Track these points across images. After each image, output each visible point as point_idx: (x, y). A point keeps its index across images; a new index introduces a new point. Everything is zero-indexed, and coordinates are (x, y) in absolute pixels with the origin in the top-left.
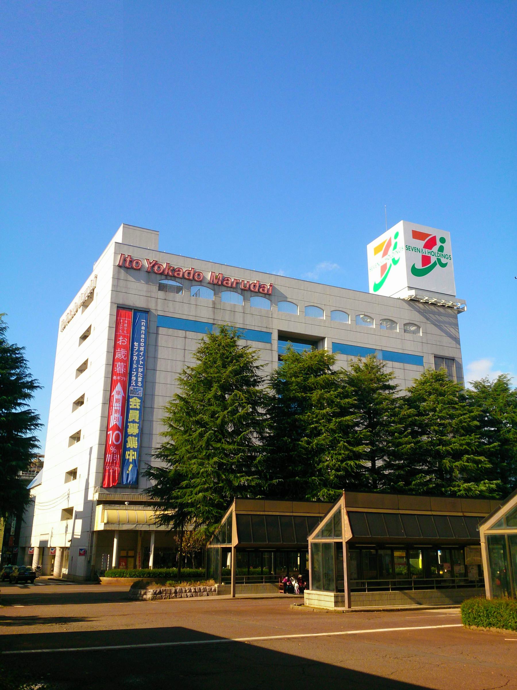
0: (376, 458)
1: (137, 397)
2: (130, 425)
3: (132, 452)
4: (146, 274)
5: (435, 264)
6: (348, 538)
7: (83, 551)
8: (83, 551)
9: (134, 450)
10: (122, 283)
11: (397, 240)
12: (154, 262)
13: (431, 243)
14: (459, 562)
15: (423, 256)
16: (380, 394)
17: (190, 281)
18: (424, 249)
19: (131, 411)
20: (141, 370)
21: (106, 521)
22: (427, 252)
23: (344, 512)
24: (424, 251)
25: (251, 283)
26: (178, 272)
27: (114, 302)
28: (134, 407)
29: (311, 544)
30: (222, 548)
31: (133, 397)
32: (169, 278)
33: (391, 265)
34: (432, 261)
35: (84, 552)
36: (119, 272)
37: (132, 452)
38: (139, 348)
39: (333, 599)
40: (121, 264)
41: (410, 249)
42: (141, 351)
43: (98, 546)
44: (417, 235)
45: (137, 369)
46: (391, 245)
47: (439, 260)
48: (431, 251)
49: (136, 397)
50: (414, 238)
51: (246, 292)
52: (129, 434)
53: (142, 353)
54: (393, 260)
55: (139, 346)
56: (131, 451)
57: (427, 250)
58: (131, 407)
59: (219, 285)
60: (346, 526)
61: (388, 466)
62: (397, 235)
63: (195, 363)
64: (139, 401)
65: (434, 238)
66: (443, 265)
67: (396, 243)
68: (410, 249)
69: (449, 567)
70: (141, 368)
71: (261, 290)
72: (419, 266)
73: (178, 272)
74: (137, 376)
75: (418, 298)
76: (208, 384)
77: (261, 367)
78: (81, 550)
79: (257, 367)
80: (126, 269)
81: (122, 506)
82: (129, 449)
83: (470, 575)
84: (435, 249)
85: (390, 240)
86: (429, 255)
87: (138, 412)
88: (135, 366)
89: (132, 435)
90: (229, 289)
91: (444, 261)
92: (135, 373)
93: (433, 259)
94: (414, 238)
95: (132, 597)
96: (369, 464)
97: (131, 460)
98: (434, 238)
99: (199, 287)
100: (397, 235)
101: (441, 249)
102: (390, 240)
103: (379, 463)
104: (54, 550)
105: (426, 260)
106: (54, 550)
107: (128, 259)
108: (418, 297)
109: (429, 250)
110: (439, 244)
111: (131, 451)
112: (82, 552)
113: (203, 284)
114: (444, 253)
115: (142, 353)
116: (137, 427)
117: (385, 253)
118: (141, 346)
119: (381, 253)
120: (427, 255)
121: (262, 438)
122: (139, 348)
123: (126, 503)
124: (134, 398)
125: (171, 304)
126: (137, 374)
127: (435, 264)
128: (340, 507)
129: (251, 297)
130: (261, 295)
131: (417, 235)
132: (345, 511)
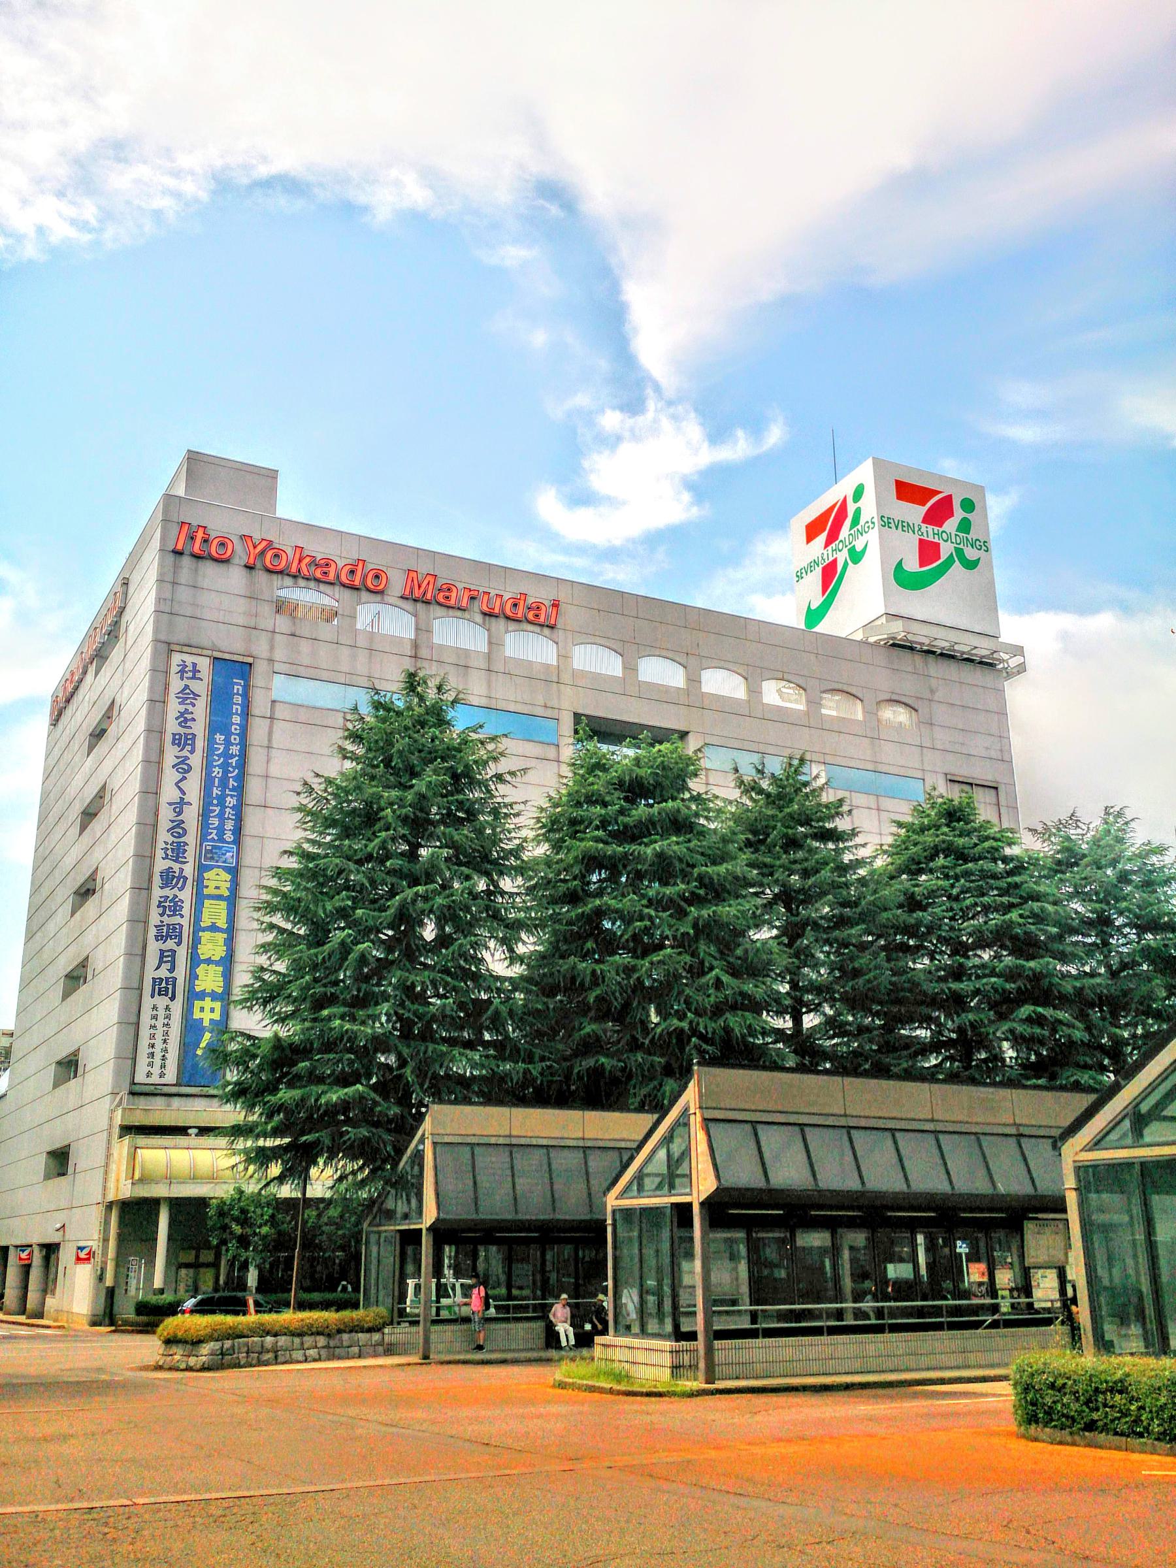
0: (804, 1010)
1: (225, 869)
2: (205, 936)
3: (208, 1003)
4: (244, 571)
5: (950, 561)
6: (706, 1190)
7: (86, 1251)
8: (86, 1251)
9: (214, 996)
10: (183, 594)
11: (858, 505)
12: (264, 544)
13: (940, 512)
14: (1009, 1260)
15: (920, 540)
16: (811, 851)
17: (355, 592)
18: (923, 526)
19: (207, 903)
20: (231, 801)
21: (137, 1176)
22: (930, 532)
23: (696, 1121)
24: (924, 529)
25: (505, 598)
26: (325, 570)
27: (163, 637)
28: (217, 892)
29: (614, 1212)
30: (400, 1231)
31: (211, 868)
32: (302, 583)
33: (846, 562)
34: (944, 555)
35: (89, 1254)
36: (176, 568)
37: (208, 1003)
38: (227, 749)
39: (667, 1360)
40: (180, 547)
41: (892, 525)
42: (232, 756)
43: (121, 1238)
44: (907, 491)
45: (222, 799)
46: (846, 516)
47: (959, 552)
48: (941, 530)
49: (219, 867)
50: (899, 497)
51: (493, 619)
52: (202, 957)
53: (233, 761)
54: (852, 551)
55: (228, 743)
56: (208, 999)
57: (930, 527)
58: (206, 891)
59: (428, 603)
60: (700, 1159)
61: (833, 1025)
62: (859, 493)
63: (337, 768)
64: (228, 877)
65: (949, 499)
66: (971, 565)
67: (858, 512)
68: (892, 525)
69: (983, 1274)
70: (232, 796)
71: (530, 616)
72: (912, 564)
73: (325, 570)
74: (221, 816)
75: (911, 642)
76: (370, 817)
77: (508, 778)
78: (81, 1248)
79: (499, 778)
80: (194, 560)
81: (180, 1140)
82: (202, 995)
83: (1037, 1294)
84: (951, 525)
85: (845, 500)
86: (936, 540)
87: (224, 904)
88: (216, 791)
89: (209, 961)
90: (451, 612)
91: (971, 553)
92: (218, 809)
93: (946, 550)
94: (899, 497)
95: (161, 1363)
96: (785, 1023)
97: (206, 1023)
98: (949, 499)
99: (379, 607)
100: (859, 493)
101: (965, 526)
102: (845, 500)
103: (810, 1021)
104: (26, 1252)
105: (928, 551)
106: (26, 1252)
107: (200, 534)
108: (910, 637)
109: (936, 528)
110: (959, 514)
111: (208, 999)
112: (82, 1255)
113: (387, 599)
114: (973, 535)
115: (233, 761)
116: (221, 942)
117: (832, 537)
118: (232, 744)
119: (823, 537)
120: (931, 539)
121: (514, 958)
122: (227, 749)
123: (190, 1131)
124: (215, 870)
125: (305, 647)
126: (222, 812)
127: (950, 561)
128: (686, 1109)
129: (507, 631)
130: (530, 627)
131: (907, 491)
132: (699, 1119)
